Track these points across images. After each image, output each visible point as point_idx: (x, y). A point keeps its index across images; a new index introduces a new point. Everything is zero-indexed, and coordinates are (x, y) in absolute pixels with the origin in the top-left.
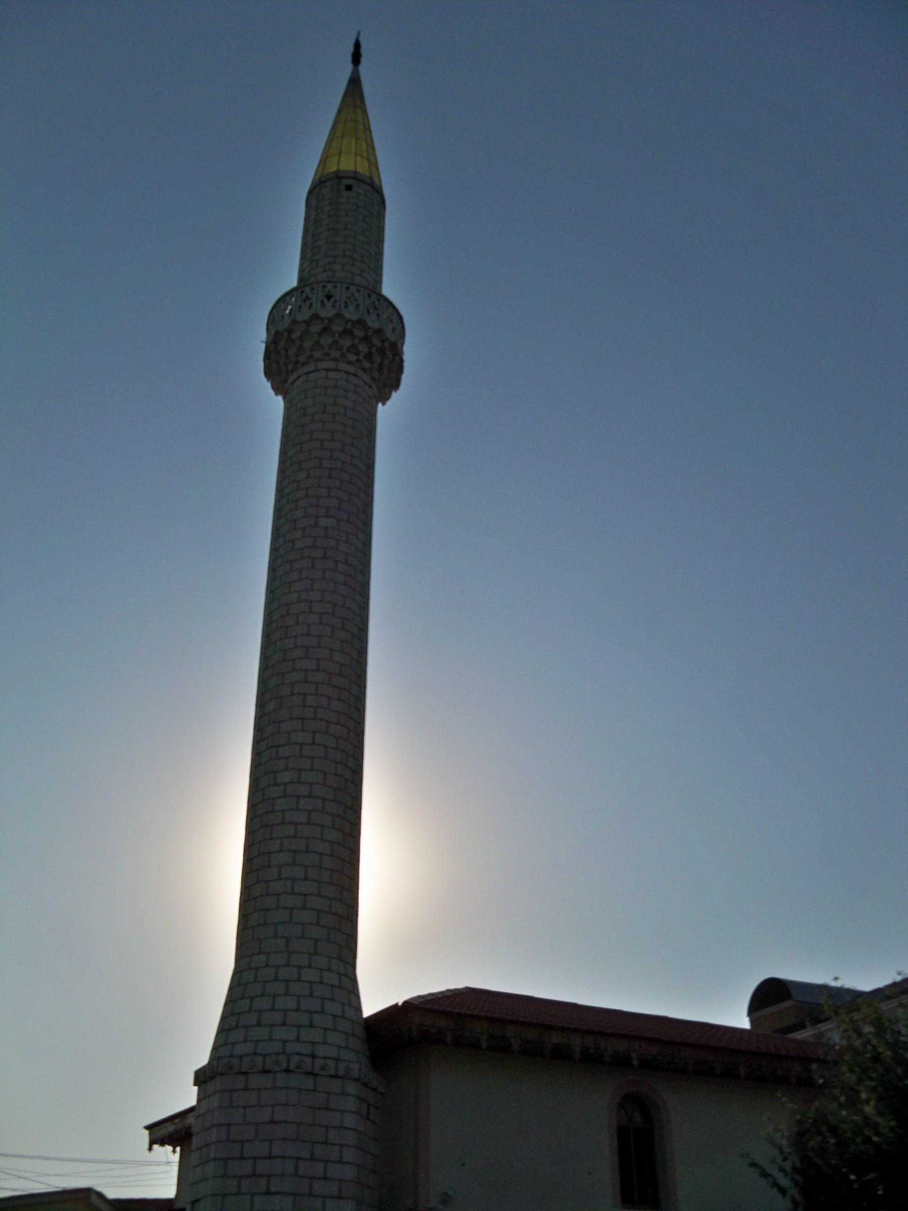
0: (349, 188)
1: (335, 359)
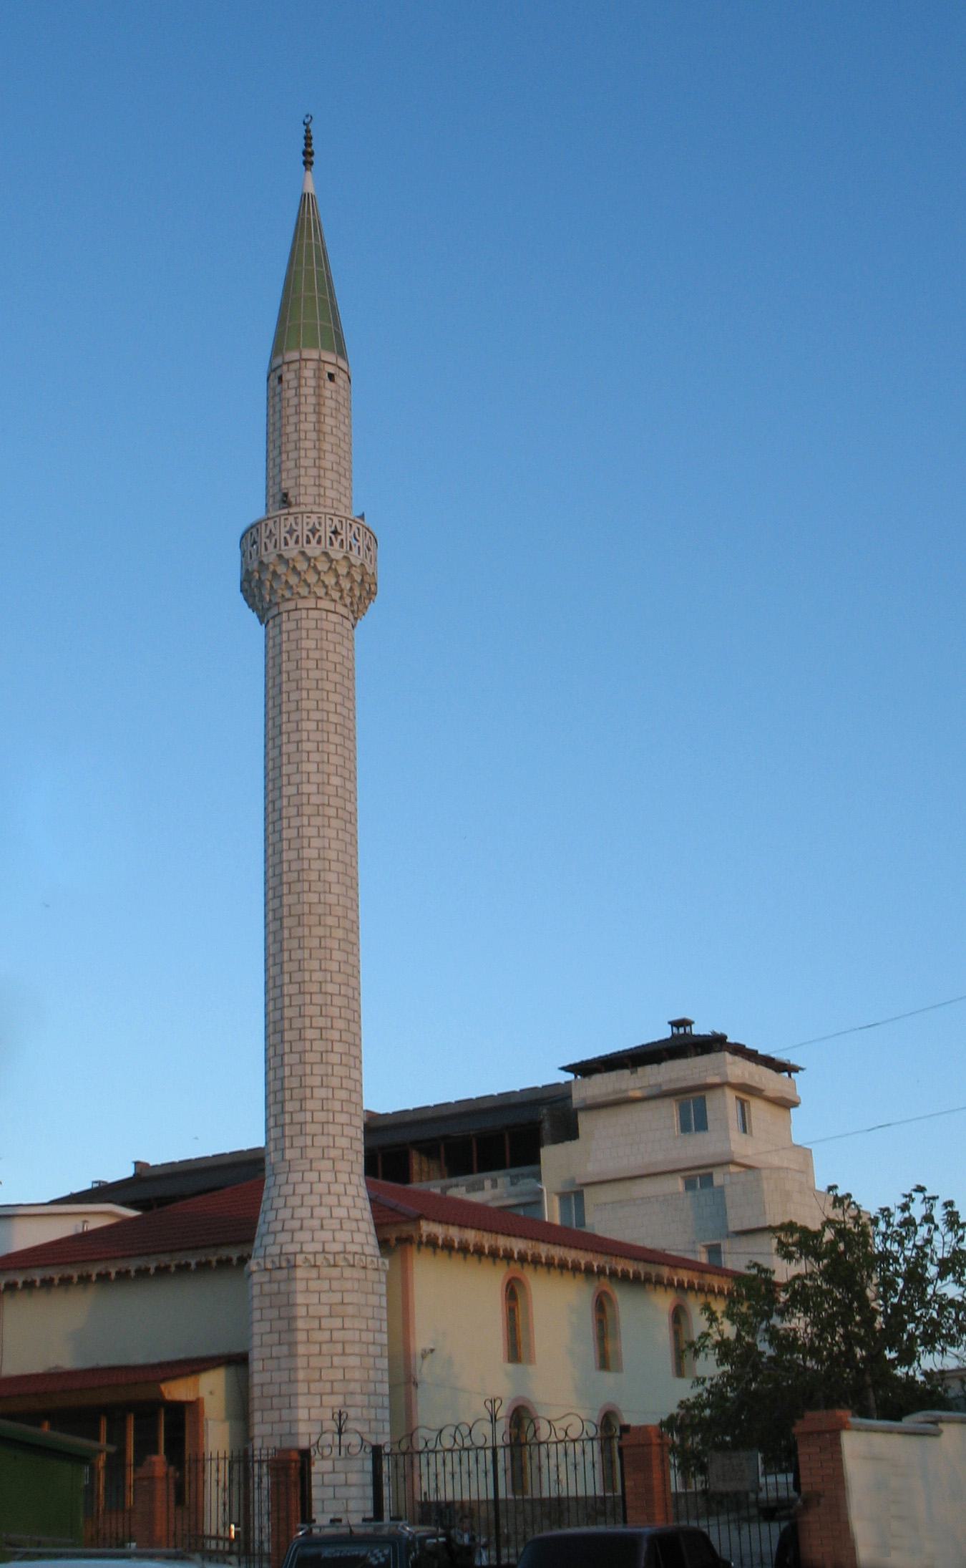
0: (331, 377)
1: (335, 601)
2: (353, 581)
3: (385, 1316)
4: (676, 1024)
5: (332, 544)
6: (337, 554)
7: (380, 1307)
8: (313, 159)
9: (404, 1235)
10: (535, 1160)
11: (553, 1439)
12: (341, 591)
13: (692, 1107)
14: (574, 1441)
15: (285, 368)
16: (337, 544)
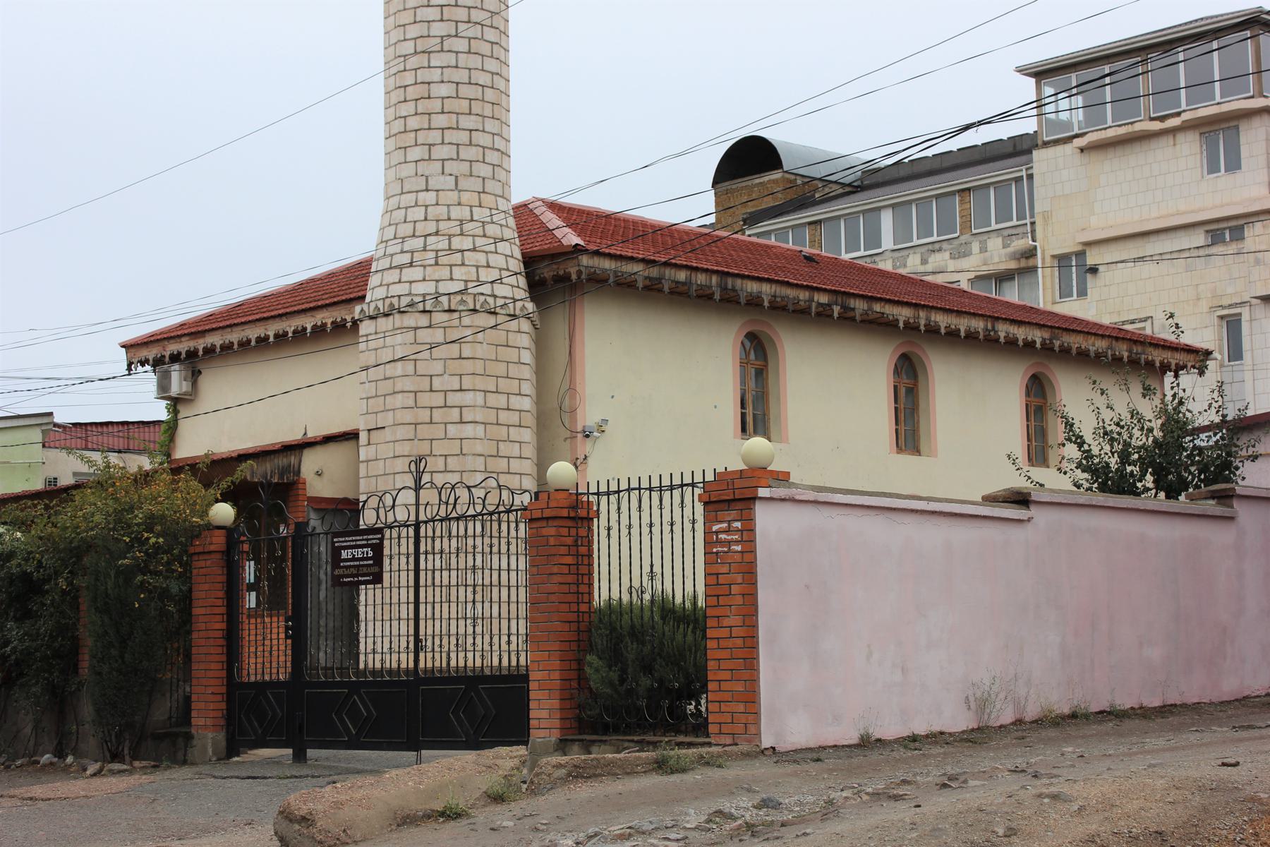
11: (471, 512)
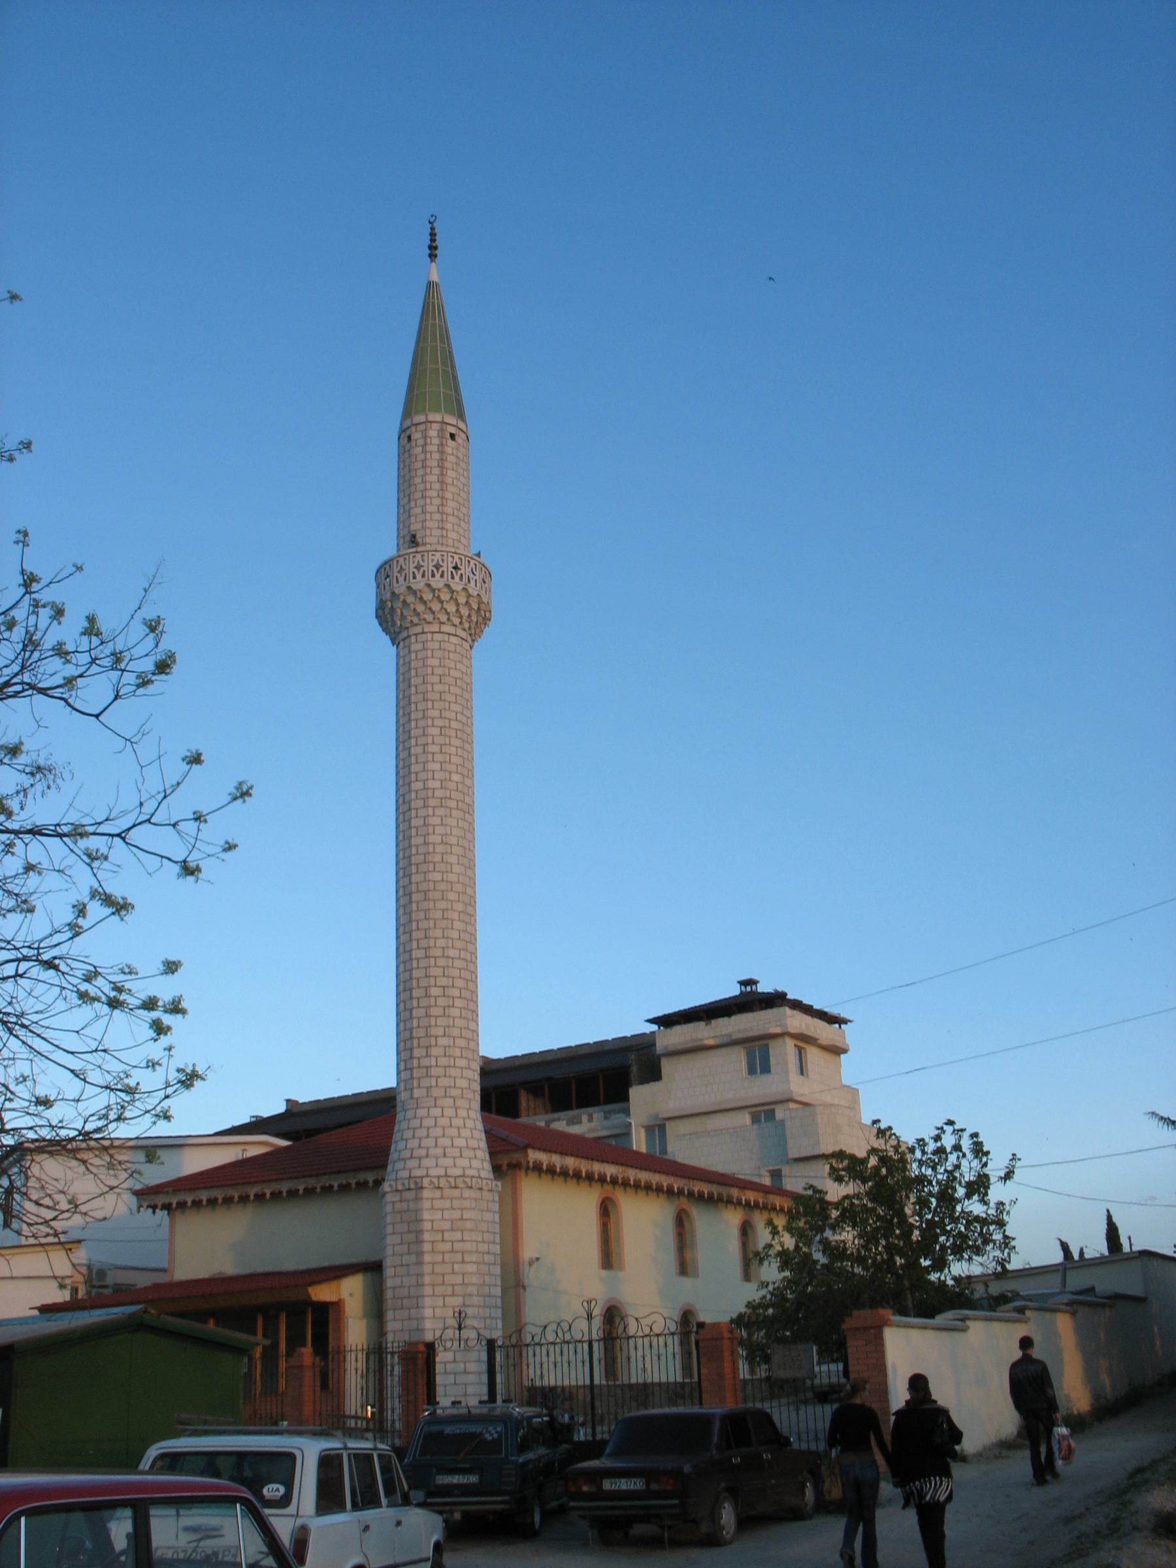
0: (452, 436)
2: (471, 609)
3: (498, 1230)
4: (744, 983)
5: (453, 578)
6: (457, 586)
7: (494, 1222)
8: (428, 252)
9: (514, 1162)
10: (625, 1098)
12: (461, 617)
13: (758, 1054)
14: (658, 1335)
15: (413, 428)
16: (457, 578)
